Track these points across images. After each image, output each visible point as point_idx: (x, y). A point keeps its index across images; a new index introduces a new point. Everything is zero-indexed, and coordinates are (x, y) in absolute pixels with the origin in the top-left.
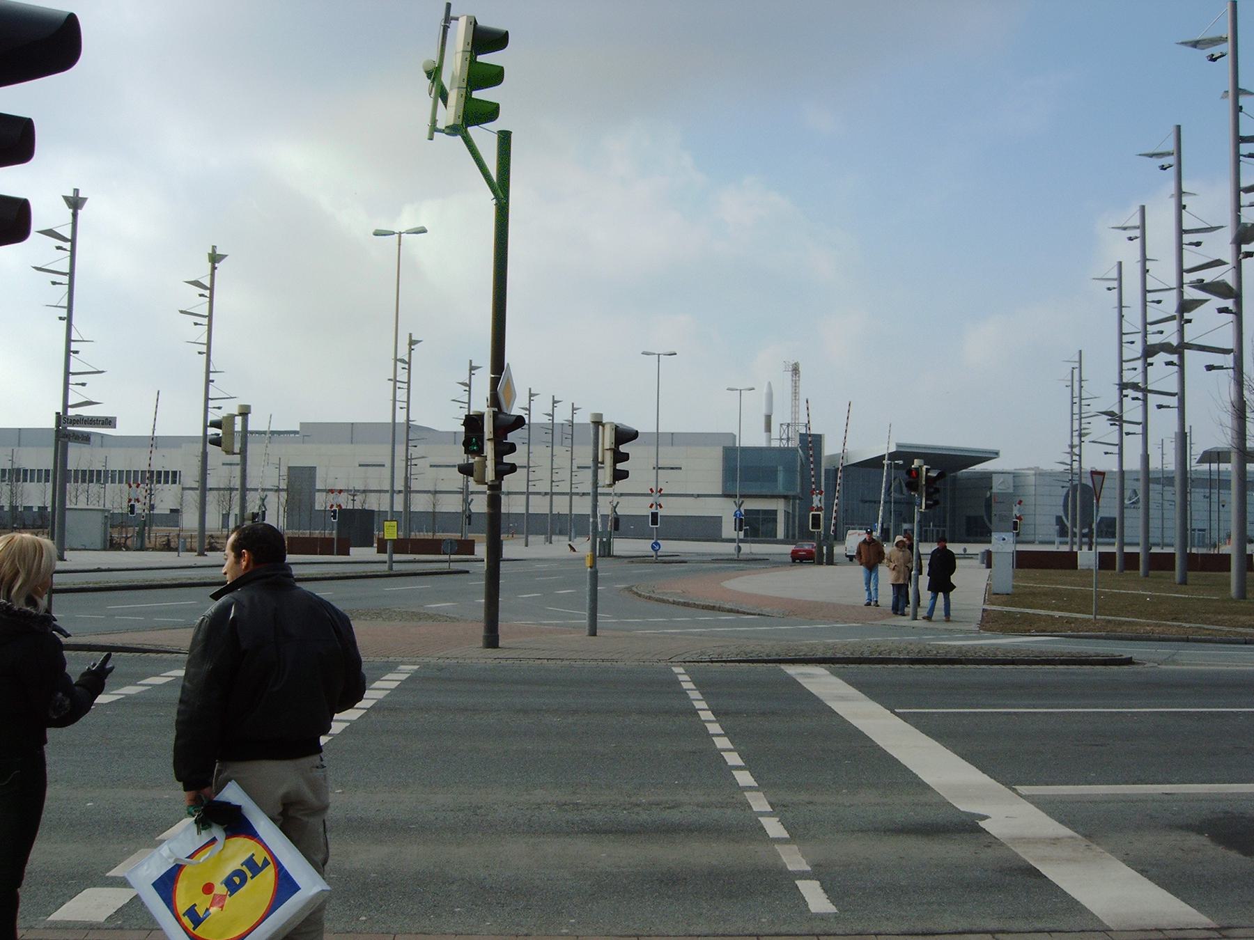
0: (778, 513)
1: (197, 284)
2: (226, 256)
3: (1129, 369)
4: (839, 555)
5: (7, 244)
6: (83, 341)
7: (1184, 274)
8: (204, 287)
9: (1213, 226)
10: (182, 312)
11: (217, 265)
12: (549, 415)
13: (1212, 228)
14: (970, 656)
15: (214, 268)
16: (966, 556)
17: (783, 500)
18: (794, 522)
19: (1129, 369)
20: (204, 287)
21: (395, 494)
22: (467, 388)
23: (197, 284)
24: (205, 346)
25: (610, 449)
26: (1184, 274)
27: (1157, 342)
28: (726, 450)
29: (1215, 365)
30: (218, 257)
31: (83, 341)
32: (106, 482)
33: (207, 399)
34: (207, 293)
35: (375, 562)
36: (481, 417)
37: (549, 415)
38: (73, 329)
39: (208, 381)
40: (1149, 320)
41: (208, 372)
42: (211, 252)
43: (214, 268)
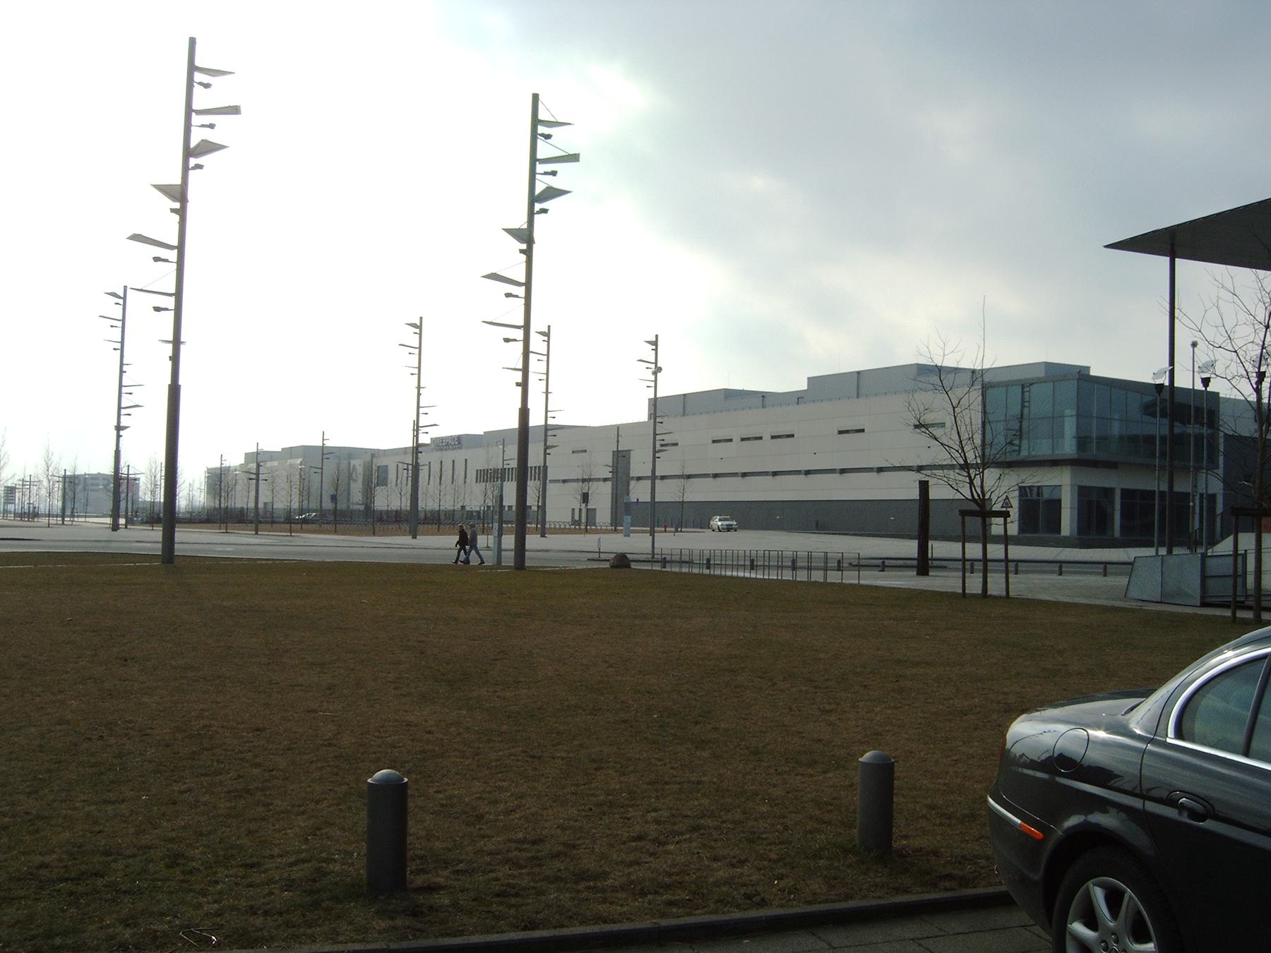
0: (1083, 484)
1: (114, 295)
4: (991, 520)
5: (1125, 381)
7: (193, 114)
8: (119, 297)
9: (559, 121)
10: (100, 316)
13: (557, 122)
15: (119, 436)
16: (358, 504)
17: (1069, 467)
18: (531, 473)
20: (119, 297)
21: (657, 481)
23: (114, 295)
24: (120, 344)
26: (193, 114)
32: (487, 481)
33: (121, 386)
34: (121, 301)
35: (588, 552)
36: (1166, 437)
39: (122, 372)
41: (122, 364)
43: (119, 436)
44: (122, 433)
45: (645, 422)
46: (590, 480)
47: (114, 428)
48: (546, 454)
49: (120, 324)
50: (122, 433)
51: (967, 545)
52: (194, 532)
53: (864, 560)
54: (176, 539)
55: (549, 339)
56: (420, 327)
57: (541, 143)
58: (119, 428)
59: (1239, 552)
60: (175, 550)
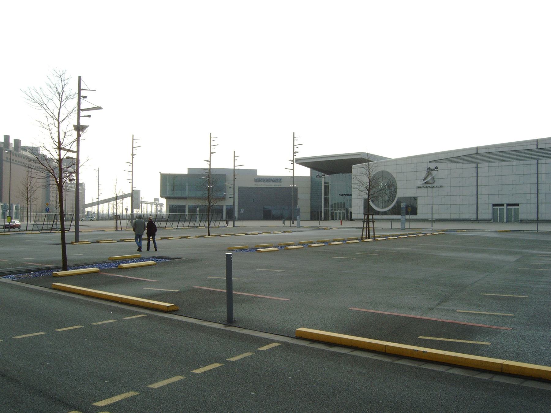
2: (136, 154)
3: (85, 116)
6: (89, 90)
7: (81, 111)
11: (81, 132)
12: (208, 161)
14: (360, 346)
15: (133, 158)
19: (85, 116)
22: (209, 163)
25: (233, 322)
26: (81, 111)
27: (454, 356)
28: (417, 197)
29: (88, 117)
30: (80, 128)
31: (89, 90)
37: (208, 161)
38: (82, 81)
40: (134, 147)
42: (76, 124)
43: (133, 158)
44: (134, 156)
45: (257, 174)
46: (516, 165)
47: (131, 155)
48: (210, 156)
49: (292, 171)
50: (134, 156)
51: (292, 175)
52: (44, 233)
53: (73, 229)
54: (61, 234)
55: (210, 163)
56: (210, 162)
57: (82, 101)
58: (133, 155)
59: (160, 206)
60: (79, 235)
